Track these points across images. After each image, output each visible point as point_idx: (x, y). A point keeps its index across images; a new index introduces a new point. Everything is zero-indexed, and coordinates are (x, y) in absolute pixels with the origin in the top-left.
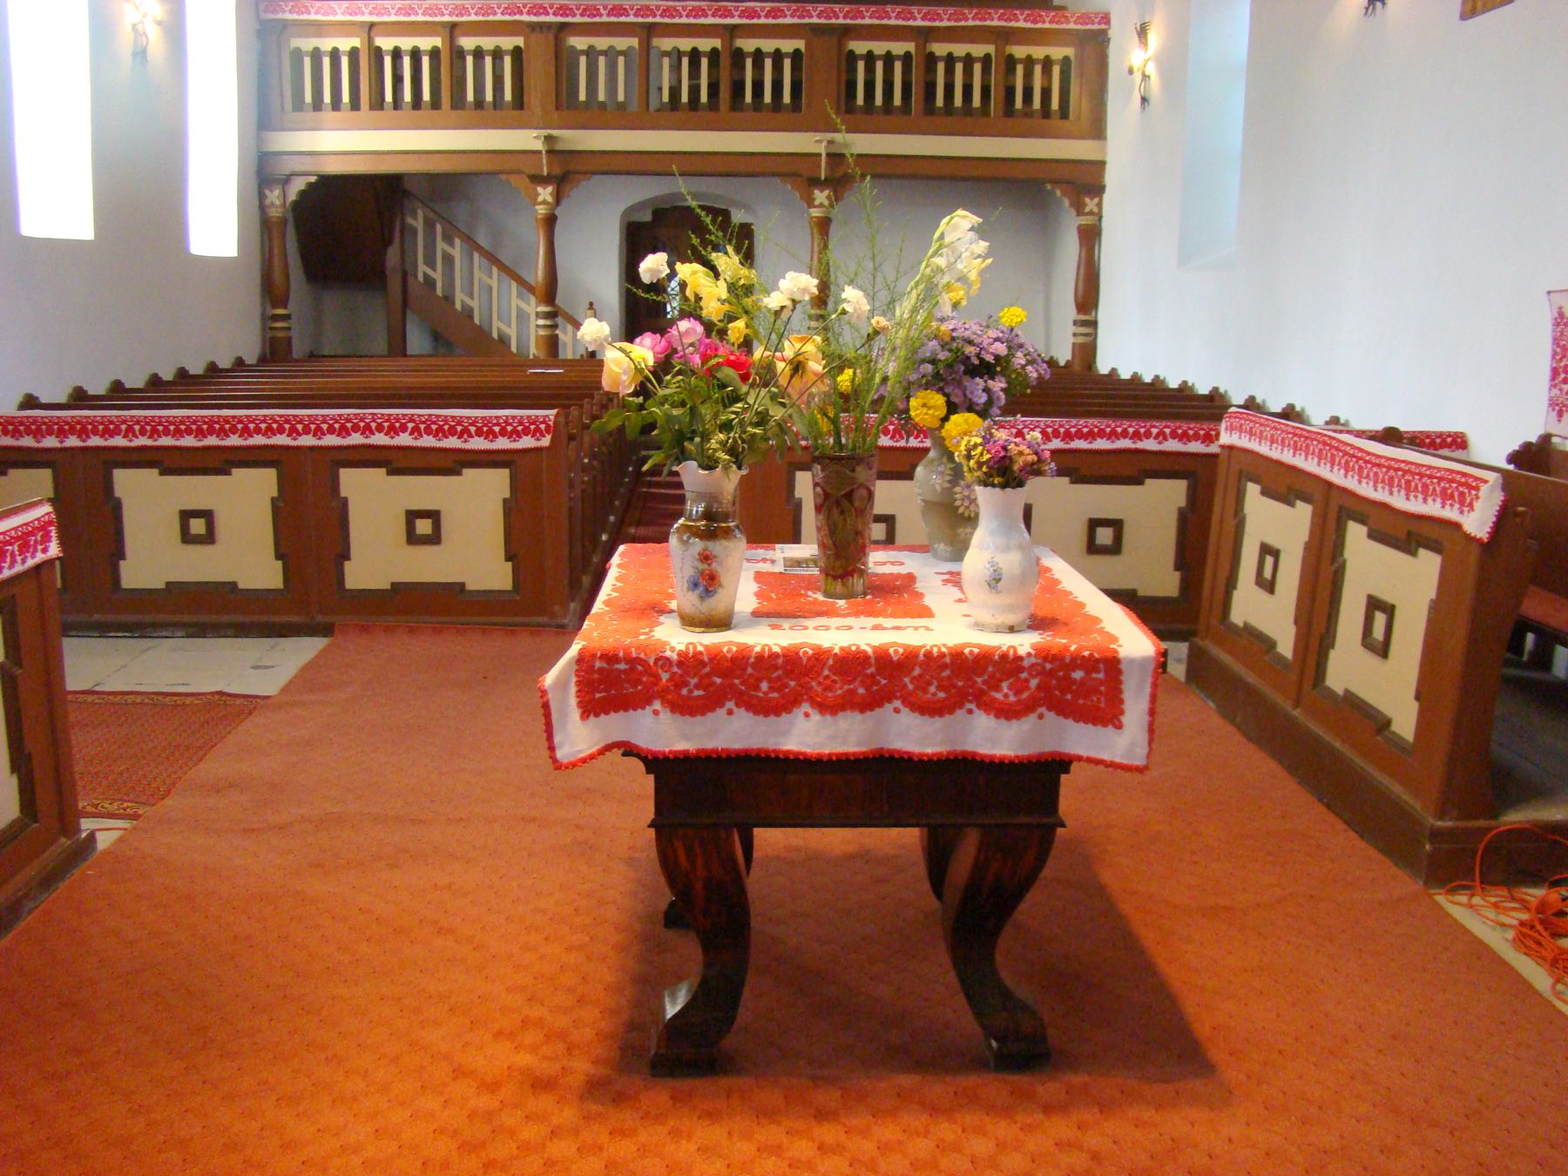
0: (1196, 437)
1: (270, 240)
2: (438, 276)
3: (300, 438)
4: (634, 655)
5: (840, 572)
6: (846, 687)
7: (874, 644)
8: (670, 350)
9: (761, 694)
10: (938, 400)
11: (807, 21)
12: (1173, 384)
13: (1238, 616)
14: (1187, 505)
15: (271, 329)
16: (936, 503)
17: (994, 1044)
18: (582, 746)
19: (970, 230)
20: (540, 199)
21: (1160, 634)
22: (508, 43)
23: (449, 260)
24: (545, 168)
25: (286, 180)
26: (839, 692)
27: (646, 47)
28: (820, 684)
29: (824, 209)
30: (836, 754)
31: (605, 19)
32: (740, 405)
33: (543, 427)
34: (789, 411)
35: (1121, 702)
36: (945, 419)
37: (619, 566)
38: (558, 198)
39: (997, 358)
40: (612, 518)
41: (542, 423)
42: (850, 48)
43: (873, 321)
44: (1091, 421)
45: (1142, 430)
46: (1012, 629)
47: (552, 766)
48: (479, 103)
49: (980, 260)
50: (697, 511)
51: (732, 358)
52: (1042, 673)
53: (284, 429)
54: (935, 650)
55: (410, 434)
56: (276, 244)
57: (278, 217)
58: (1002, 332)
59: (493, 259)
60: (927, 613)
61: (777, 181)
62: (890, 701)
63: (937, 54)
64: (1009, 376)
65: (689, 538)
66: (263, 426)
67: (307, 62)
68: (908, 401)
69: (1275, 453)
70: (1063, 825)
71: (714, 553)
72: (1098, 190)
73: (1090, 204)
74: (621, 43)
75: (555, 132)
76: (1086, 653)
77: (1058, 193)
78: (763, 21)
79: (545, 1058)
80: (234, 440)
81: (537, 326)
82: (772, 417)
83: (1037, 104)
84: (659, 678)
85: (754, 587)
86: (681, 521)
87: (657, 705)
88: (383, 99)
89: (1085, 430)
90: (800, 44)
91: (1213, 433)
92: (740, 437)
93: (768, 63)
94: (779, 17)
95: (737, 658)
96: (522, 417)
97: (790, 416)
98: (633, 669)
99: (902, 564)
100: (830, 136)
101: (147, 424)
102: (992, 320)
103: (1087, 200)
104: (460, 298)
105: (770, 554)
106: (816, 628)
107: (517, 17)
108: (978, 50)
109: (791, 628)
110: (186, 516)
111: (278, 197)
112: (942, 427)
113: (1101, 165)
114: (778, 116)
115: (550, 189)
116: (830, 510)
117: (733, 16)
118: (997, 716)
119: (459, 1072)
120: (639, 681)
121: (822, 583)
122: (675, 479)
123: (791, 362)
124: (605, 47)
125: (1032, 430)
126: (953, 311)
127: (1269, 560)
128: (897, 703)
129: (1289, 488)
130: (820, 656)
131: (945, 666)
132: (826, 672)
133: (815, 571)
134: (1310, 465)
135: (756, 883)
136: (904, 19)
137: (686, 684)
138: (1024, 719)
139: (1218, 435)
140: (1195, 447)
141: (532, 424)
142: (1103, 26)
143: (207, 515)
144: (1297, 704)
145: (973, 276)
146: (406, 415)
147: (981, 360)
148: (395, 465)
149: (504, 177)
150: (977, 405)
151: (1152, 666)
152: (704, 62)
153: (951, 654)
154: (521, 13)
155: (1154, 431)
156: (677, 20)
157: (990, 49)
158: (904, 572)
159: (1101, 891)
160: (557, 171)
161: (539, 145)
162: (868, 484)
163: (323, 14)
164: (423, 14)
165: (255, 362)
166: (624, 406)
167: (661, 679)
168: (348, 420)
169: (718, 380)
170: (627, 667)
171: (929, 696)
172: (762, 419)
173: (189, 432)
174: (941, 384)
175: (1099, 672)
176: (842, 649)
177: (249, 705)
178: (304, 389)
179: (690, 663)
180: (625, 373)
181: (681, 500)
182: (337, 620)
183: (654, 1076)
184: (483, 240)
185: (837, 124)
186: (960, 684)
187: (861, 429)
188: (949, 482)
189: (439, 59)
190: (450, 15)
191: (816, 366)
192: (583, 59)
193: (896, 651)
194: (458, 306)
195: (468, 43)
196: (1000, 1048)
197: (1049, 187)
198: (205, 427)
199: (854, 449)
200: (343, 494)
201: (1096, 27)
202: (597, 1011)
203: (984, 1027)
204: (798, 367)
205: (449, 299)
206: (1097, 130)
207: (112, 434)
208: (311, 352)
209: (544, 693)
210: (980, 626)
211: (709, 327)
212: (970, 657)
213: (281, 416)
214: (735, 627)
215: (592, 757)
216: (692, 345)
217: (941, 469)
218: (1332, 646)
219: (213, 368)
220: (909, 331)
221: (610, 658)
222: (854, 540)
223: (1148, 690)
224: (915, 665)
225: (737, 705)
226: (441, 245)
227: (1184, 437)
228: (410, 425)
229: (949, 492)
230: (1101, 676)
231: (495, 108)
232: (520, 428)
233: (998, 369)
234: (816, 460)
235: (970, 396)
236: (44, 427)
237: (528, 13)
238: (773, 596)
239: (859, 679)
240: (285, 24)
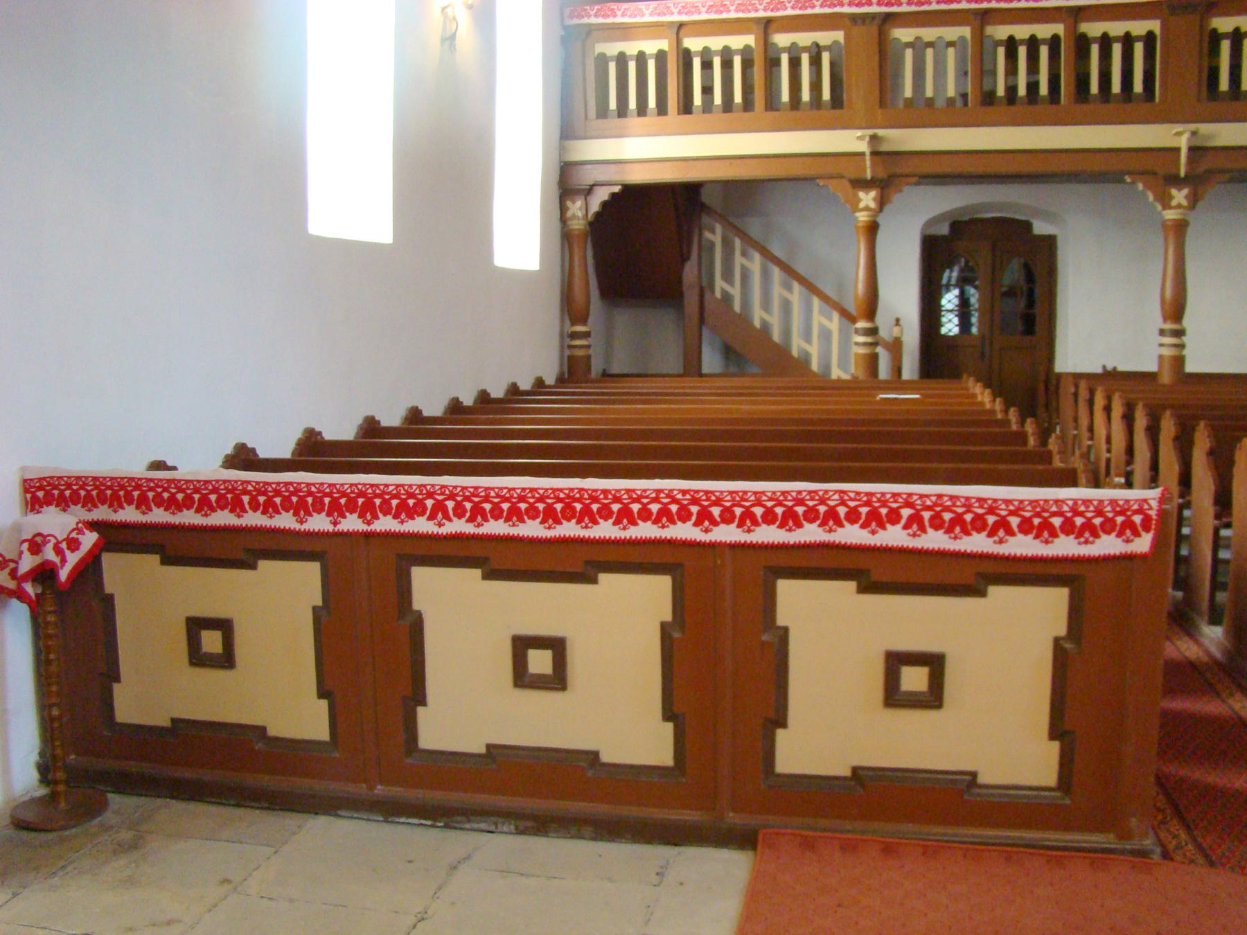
2: (735, 292)
3: (715, 529)
15: (570, 347)
20: (862, 205)
25: (589, 191)
33: (1137, 519)
38: (882, 202)
41: (1137, 512)
53: (690, 514)
57: (579, 230)
66: (655, 508)
67: (612, 67)
74: (737, 42)
77: (1140, 186)
80: (606, 530)
81: (857, 344)
96: (1101, 502)
100: (1193, 127)
101: (467, 499)
110: (522, 645)
111: (580, 209)
114: (1129, 107)
124: (911, 39)
143: (557, 646)
146: (899, 495)
148: (875, 577)
160: (882, 174)
161: (863, 147)
163: (630, 16)
168: (800, 502)
173: (532, 513)
184: (777, 250)
192: (909, 54)
195: (782, 40)
198: (559, 506)
200: (781, 621)
207: (412, 513)
208: (604, 370)
213: (684, 492)
219: (514, 390)
226: (739, 260)
228: (906, 513)
232: (1097, 521)
236: (310, 500)
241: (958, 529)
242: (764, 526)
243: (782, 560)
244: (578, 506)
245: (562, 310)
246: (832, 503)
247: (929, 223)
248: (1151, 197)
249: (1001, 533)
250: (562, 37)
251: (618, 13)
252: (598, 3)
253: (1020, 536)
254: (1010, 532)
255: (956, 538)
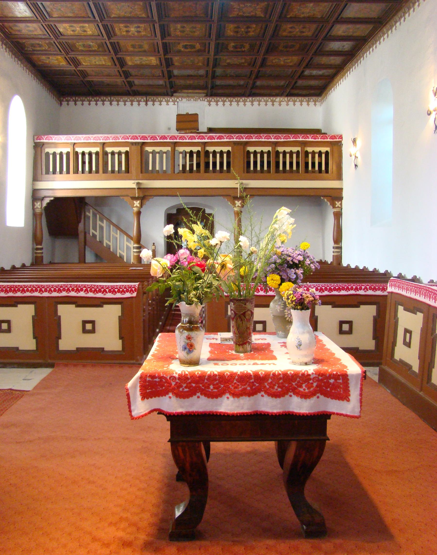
0: (379, 289)
1: (36, 220)
2: (97, 234)
4: (162, 375)
5: (241, 343)
6: (243, 387)
7: (253, 370)
8: (177, 261)
9: (210, 390)
10: (278, 277)
11: (232, 140)
12: (371, 269)
13: (397, 356)
14: (376, 315)
16: (278, 317)
17: (304, 527)
18: (142, 411)
19: (287, 214)
20: (135, 205)
21: (363, 364)
22: (123, 149)
23: (101, 228)
24: (137, 194)
25: (42, 199)
26: (240, 389)
27: (174, 150)
28: (232, 386)
29: (239, 208)
30: (239, 413)
31: (159, 141)
32: (201, 280)
33: (133, 289)
34: (220, 283)
35: (349, 391)
36: (280, 285)
37: (158, 341)
39: (299, 261)
40: (161, 323)
41: (133, 288)
42: (248, 150)
43: (251, 249)
44: (339, 284)
45: (358, 287)
46: (306, 364)
47: (130, 418)
48: (113, 171)
49: (291, 225)
50: (186, 320)
51: (199, 263)
52: (318, 380)
54: (277, 372)
55: (84, 292)
56: (38, 222)
58: (301, 252)
59: (117, 227)
60: (274, 358)
61: (222, 198)
62: (260, 392)
63: (280, 151)
64: (304, 268)
65: (183, 331)
66: (30, 289)
67: (51, 157)
68: (266, 278)
69: (408, 294)
70: (329, 440)
71: (192, 336)
72: (340, 199)
73: (338, 204)
74: (165, 149)
75: (140, 181)
76: (335, 373)
77: (326, 200)
78: (216, 140)
79: (128, 533)
80: (19, 294)
81: (134, 252)
82: (214, 285)
83: (317, 168)
84: (171, 384)
85: (209, 349)
86: (180, 324)
87: (170, 394)
88: (78, 170)
89: (337, 287)
90: (230, 148)
91: (385, 287)
92: (201, 293)
93: (218, 155)
94: (222, 139)
95: (201, 376)
97: (221, 284)
98: (161, 381)
99: (266, 339)
102: (297, 247)
103: (336, 202)
104: (105, 242)
105: (215, 336)
106: (231, 364)
107: (127, 140)
108: (295, 149)
109: (222, 365)
111: (39, 205)
112: (279, 287)
113: (341, 189)
115: (139, 202)
116: (237, 320)
117: (205, 139)
118: (301, 398)
119: (94, 539)
120: (163, 386)
121: (234, 347)
122: (177, 308)
123: (220, 264)
124: (182, 151)
125: (312, 288)
126: (282, 244)
127: (408, 335)
128: (263, 393)
129: (414, 307)
130: (232, 375)
131: (281, 379)
132: (235, 381)
133: (232, 343)
134: (421, 298)
135: (211, 465)
136: (267, 139)
137: (182, 386)
138: (311, 398)
139: (387, 288)
140: (379, 293)
141: (129, 288)
142: (340, 140)
144: (421, 390)
145: (289, 231)
147: (294, 262)
149: (122, 198)
150: (292, 279)
151: (360, 377)
152: (195, 155)
153: (283, 374)
154: (128, 139)
155: (363, 287)
156: (185, 141)
157: (299, 149)
158: (266, 343)
159: (346, 465)
160: (141, 195)
161: (134, 186)
162: (251, 310)
164: (93, 140)
165: (29, 265)
166: (158, 281)
167: (172, 385)
168: (61, 287)
169: (193, 271)
170: (159, 380)
171: (275, 390)
172: (210, 286)
174: (278, 272)
175: (340, 380)
176: (241, 372)
177: (22, 393)
178: (47, 275)
179: (183, 378)
180: (159, 269)
181: (180, 316)
182: (56, 362)
183: (171, 540)
184: (114, 221)
185: (236, 177)
186: (287, 385)
187: (248, 289)
188: (282, 308)
189: (99, 155)
190: (103, 140)
191: (230, 266)
192: (151, 155)
193: (262, 373)
194: (105, 245)
195: (109, 150)
196: (306, 529)
197: (322, 198)
198: (8, 289)
199: (246, 296)
200: (59, 314)
201: (337, 140)
202: (149, 514)
203: (301, 521)
204: (223, 266)
205: (101, 242)
206: (339, 177)
208: (51, 261)
209: (127, 390)
210: (294, 363)
211: (191, 251)
212: (290, 375)
214: (200, 365)
215: (146, 415)
216: (185, 258)
217: (279, 303)
218: (433, 367)
219: (14, 267)
220: (265, 252)
221: (153, 376)
222: (246, 331)
223: (359, 386)
224: (269, 378)
225: (201, 394)
226: (98, 222)
227: (374, 289)
228: (84, 289)
229: (283, 312)
230: (341, 381)
231: (119, 173)
232: (125, 290)
233: (300, 265)
234: (231, 301)
235: (289, 276)
237: (131, 139)
238: (216, 352)
239: (248, 384)
240: (43, 144)
241: (95, 292)
242: (54, 292)
243: (59, 300)
244: (13, 289)
245: (33, 241)
246: (68, 287)
247: (168, 209)
248: (229, 203)
249: (105, 293)
250: (34, 146)
251: (53, 139)
252: (47, 135)
253: (109, 293)
254: (106, 292)
255: (95, 294)
